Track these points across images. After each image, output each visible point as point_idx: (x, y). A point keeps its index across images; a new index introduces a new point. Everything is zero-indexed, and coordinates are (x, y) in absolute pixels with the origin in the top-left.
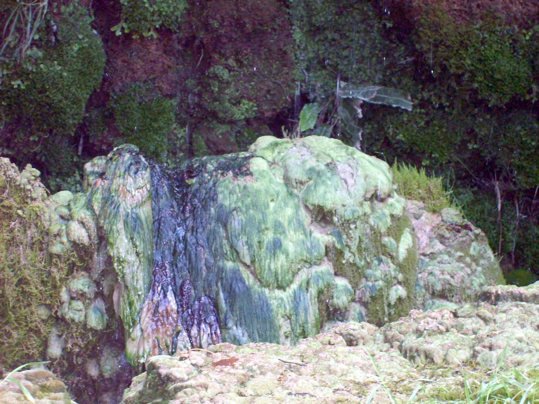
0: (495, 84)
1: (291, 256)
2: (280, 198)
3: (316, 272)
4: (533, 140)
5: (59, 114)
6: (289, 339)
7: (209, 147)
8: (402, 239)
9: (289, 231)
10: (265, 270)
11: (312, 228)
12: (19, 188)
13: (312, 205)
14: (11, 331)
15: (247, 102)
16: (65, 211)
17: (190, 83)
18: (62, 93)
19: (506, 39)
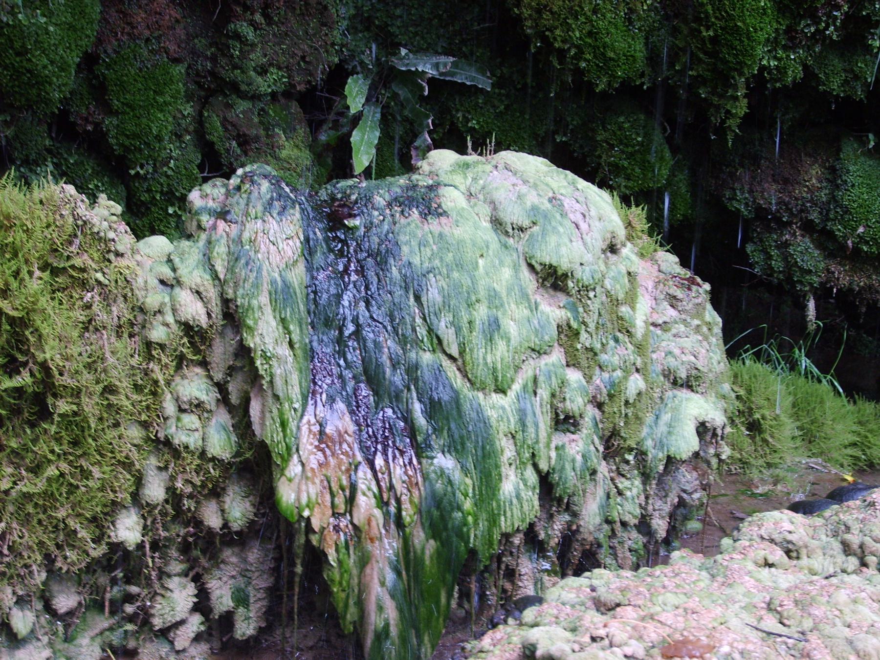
0: (606, 64)
1: (514, 342)
2: (491, 252)
3: (546, 364)
4: (638, 135)
5: (43, 85)
6: (513, 467)
7: (226, 130)
8: (638, 305)
9: (509, 303)
10: (478, 365)
11: (539, 298)
12: (97, 238)
13: (541, 264)
14: (91, 468)
15: (275, 71)
16: (166, 272)
17: (200, 43)
18: (47, 55)
19: (621, 8)
